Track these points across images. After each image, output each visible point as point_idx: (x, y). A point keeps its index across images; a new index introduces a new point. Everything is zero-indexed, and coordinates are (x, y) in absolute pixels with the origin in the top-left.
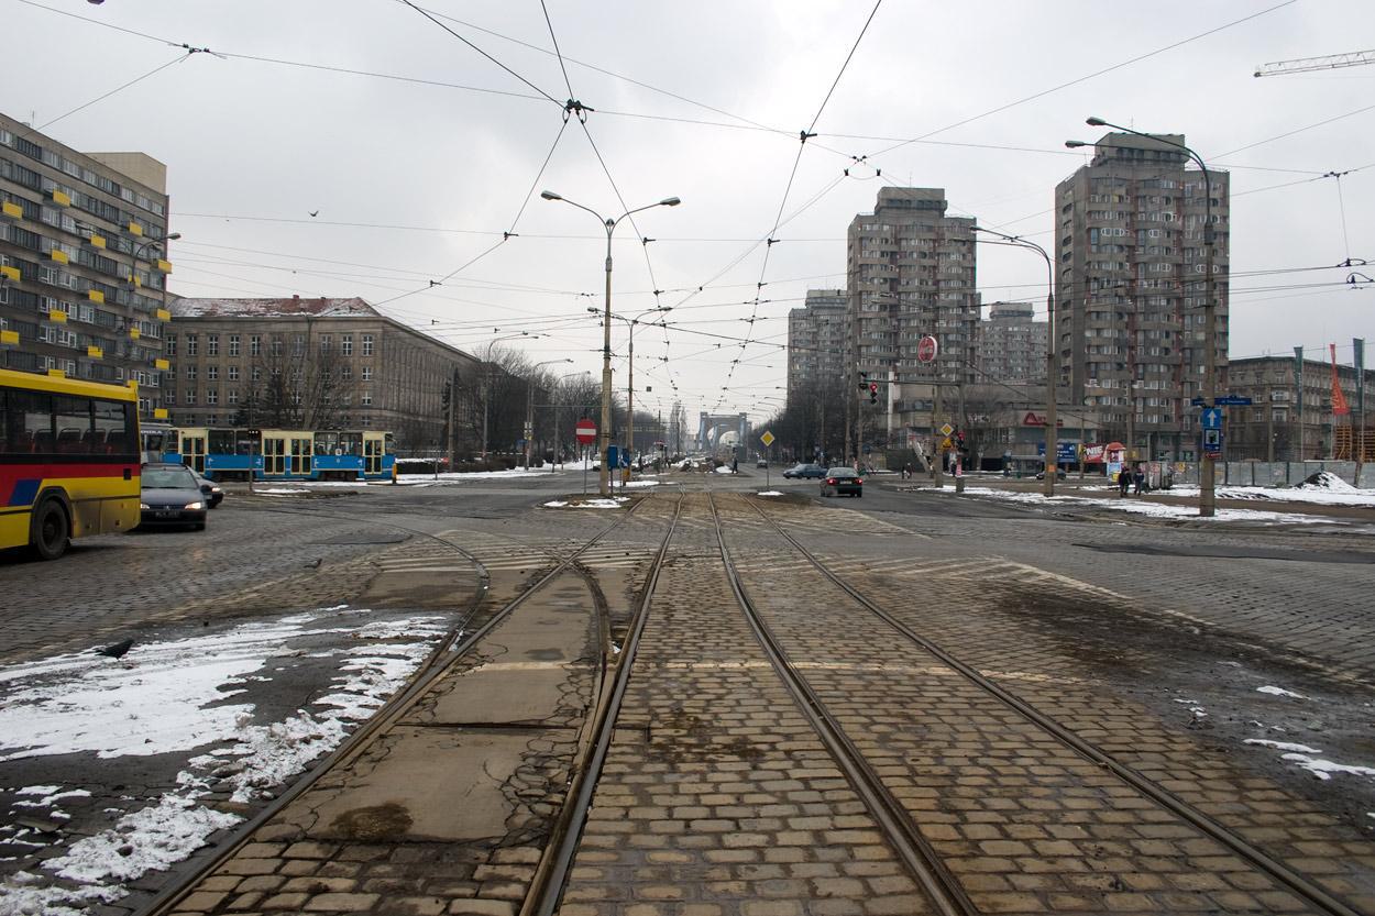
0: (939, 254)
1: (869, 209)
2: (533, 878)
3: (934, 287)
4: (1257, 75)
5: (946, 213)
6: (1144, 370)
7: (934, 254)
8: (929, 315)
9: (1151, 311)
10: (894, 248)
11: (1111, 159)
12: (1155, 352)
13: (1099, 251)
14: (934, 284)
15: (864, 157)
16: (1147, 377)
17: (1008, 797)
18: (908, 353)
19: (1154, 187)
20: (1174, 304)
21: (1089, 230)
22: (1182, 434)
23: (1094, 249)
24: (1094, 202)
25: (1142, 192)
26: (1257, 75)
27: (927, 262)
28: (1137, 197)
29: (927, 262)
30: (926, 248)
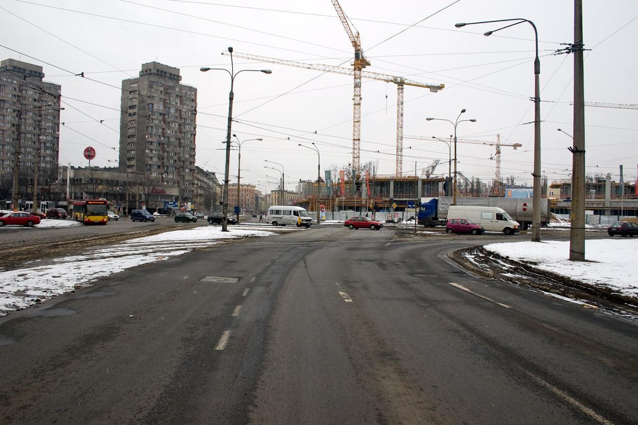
0: (42, 101)
1: (136, 75)
3: (40, 118)
4: (222, 54)
5: (43, 79)
7: (40, 100)
8: (37, 131)
9: (169, 143)
10: (19, 94)
12: (172, 162)
14: (39, 116)
18: (25, 151)
20: (178, 141)
21: (149, 104)
25: (169, 91)
26: (222, 54)
27: (37, 104)
29: (37, 104)
30: (36, 97)
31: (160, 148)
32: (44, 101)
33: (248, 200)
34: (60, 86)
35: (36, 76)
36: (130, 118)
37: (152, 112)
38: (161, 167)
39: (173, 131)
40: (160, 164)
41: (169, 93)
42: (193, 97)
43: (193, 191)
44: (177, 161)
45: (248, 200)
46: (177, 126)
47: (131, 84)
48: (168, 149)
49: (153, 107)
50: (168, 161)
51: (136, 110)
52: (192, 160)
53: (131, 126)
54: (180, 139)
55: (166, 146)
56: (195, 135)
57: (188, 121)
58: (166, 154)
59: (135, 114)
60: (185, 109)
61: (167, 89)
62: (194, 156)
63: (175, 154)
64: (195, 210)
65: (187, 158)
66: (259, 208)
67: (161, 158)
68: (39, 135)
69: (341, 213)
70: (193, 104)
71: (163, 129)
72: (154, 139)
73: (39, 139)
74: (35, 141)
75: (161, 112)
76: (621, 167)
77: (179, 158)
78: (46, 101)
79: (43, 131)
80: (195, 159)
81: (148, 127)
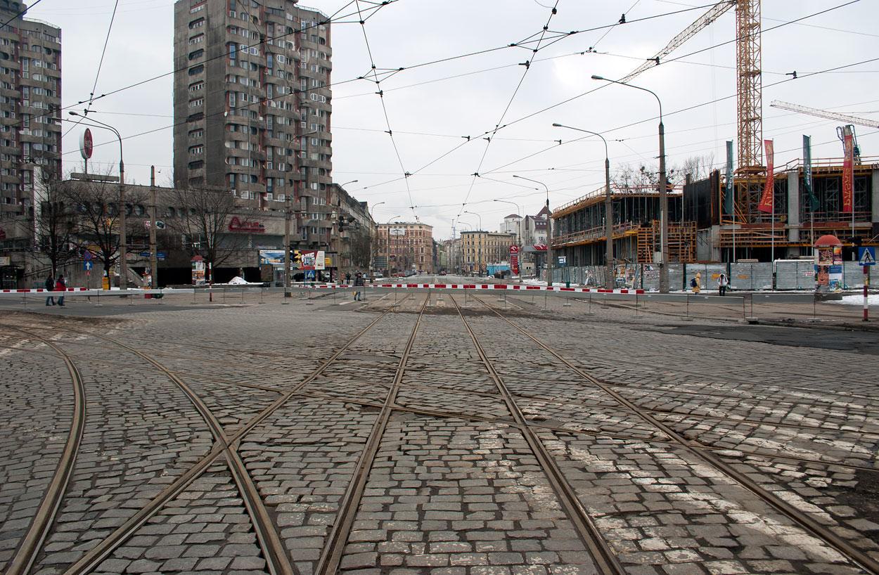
0: (21, 58)
2: (257, 537)
3: (18, 92)
6: (273, 183)
8: (13, 119)
9: (276, 130)
13: (237, 65)
14: (16, 89)
16: (276, 191)
19: (280, 16)
20: (293, 126)
21: (229, 43)
22: (301, 243)
23: (232, 63)
24: (233, 17)
25: (272, 19)
31: (256, 138)
32: (26, 59)
33: (422, 249)
34: (59, 30)
35: (8, 10)
36: (191, 79)
37: (237, 60)
38: (261, 179)
39: (282, 103)
40: (257, 172)
41: (273, 24)
42: (324, 36)
43: (329, 229)
44: (294, 168)
45: (422, 249)
47: (191, 8)
48: (273, 142)
49: (237, 50)
50: (275, 167)
51: (202, 59)
52: (324, 165)
53: (194, 95)
54: (298, 121)
55: (268, 135)
56: (329, 113)
57: (315, 84)
58: (269, 152)
59: (200, 68)
60: (306, 57)
61: (268, 14)
62: (329, 156)
63: (289, 152)
64: (336, 269)
65: (315, 161)
66: (438, 263)
67: (259, 160)
68: (18, 128)
69: (802, 267)
70: (323, 48)
71: (262, 99)
72: (244, 118)
73: (18, 135)
74: (10, 139)
75: (256, 62)
76: (806, 140)
77: (298, 160)
78: (29, 59)
79: (26, 118)
80: (331, 63)
81: (228, 92)
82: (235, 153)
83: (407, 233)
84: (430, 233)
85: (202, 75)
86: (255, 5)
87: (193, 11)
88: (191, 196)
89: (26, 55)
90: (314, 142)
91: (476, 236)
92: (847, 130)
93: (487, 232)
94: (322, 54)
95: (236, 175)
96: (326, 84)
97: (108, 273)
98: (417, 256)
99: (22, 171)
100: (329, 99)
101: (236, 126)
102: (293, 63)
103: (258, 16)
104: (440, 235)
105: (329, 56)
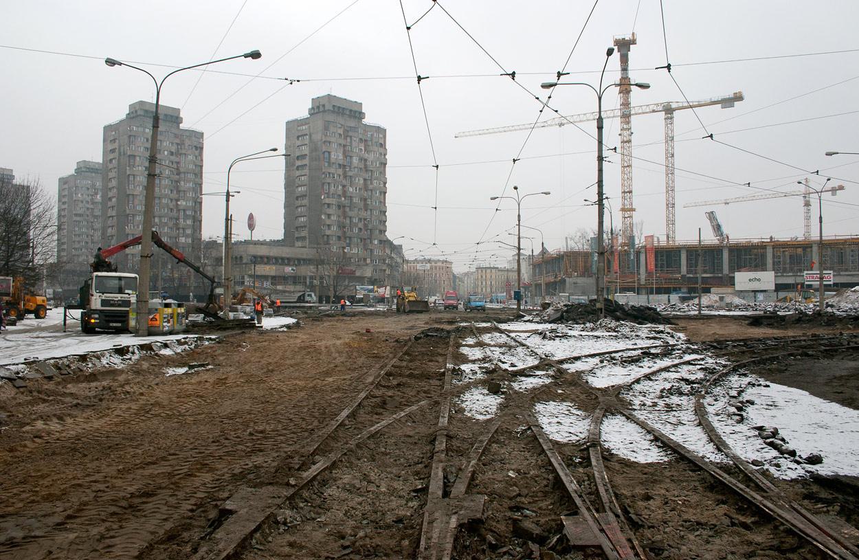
3: (178, 177)
5: (181, 125)
7: (178, 154)
9: (352, 206)
11: (140, 115)
12: (356, 230)
15: (291, 83)
16: (352, 246)
17: (642, 425)
20: (363, 203)
23: (326, 164)
25: (350, 134)
28: (347, 136)
30: (173, 149)
36: (298, 173)
37: (329, 163)
38: (343, 238)
40: (340, 234)
43: (385, 270)
46: (362, 182)
48: (350, 214)
49: (330, 157)
51: (306, 161)
52: (382, 228)
54: (365, 200)
56: (385, 193)
57: (376, 174)
60: (371, 157)
61: (348, 131)
63: (360, 220)
67: (342, 226)
68: (177, 200)
70: (381, 150)
71: (344, 186)
76: (700, 229)
82: (328, 222)
83: (431, 268)
84: (451, 268)
85: (306, 171)
86: (340, 126)
87: (299, 128)
88: (302, 250)
89: (183, 152)
90: (376, 213)
91: (488, 271)
92: (711, 215)
93: (498, 268)
94: (381, 154)
95: (328, 236)
96: (383, 173)
97: (700, 301)
98: (440, 287)
99: (178, 229)
100: (385, 183)
101: (329, 205)
102: (363, 162)
103: (342, 133)
104: (458, 269)
105: (385, 155)
